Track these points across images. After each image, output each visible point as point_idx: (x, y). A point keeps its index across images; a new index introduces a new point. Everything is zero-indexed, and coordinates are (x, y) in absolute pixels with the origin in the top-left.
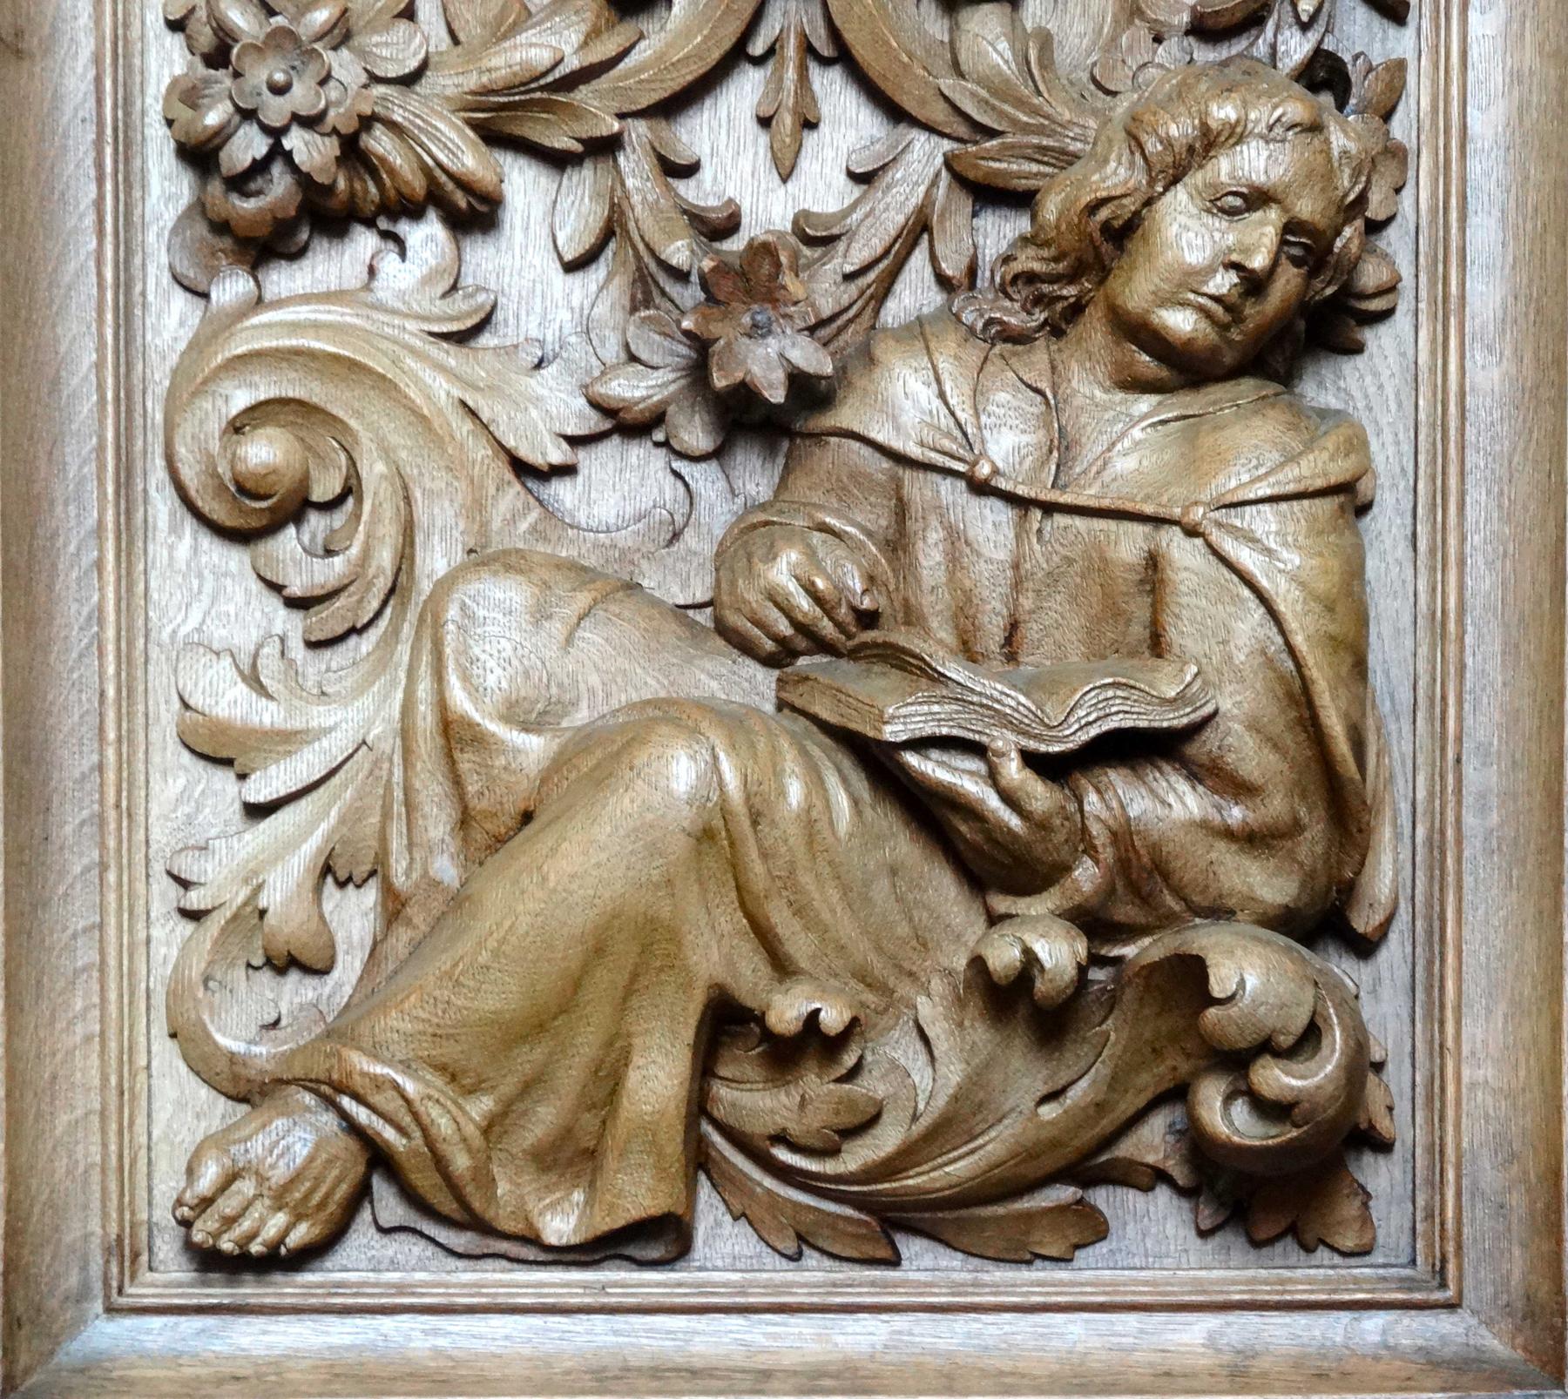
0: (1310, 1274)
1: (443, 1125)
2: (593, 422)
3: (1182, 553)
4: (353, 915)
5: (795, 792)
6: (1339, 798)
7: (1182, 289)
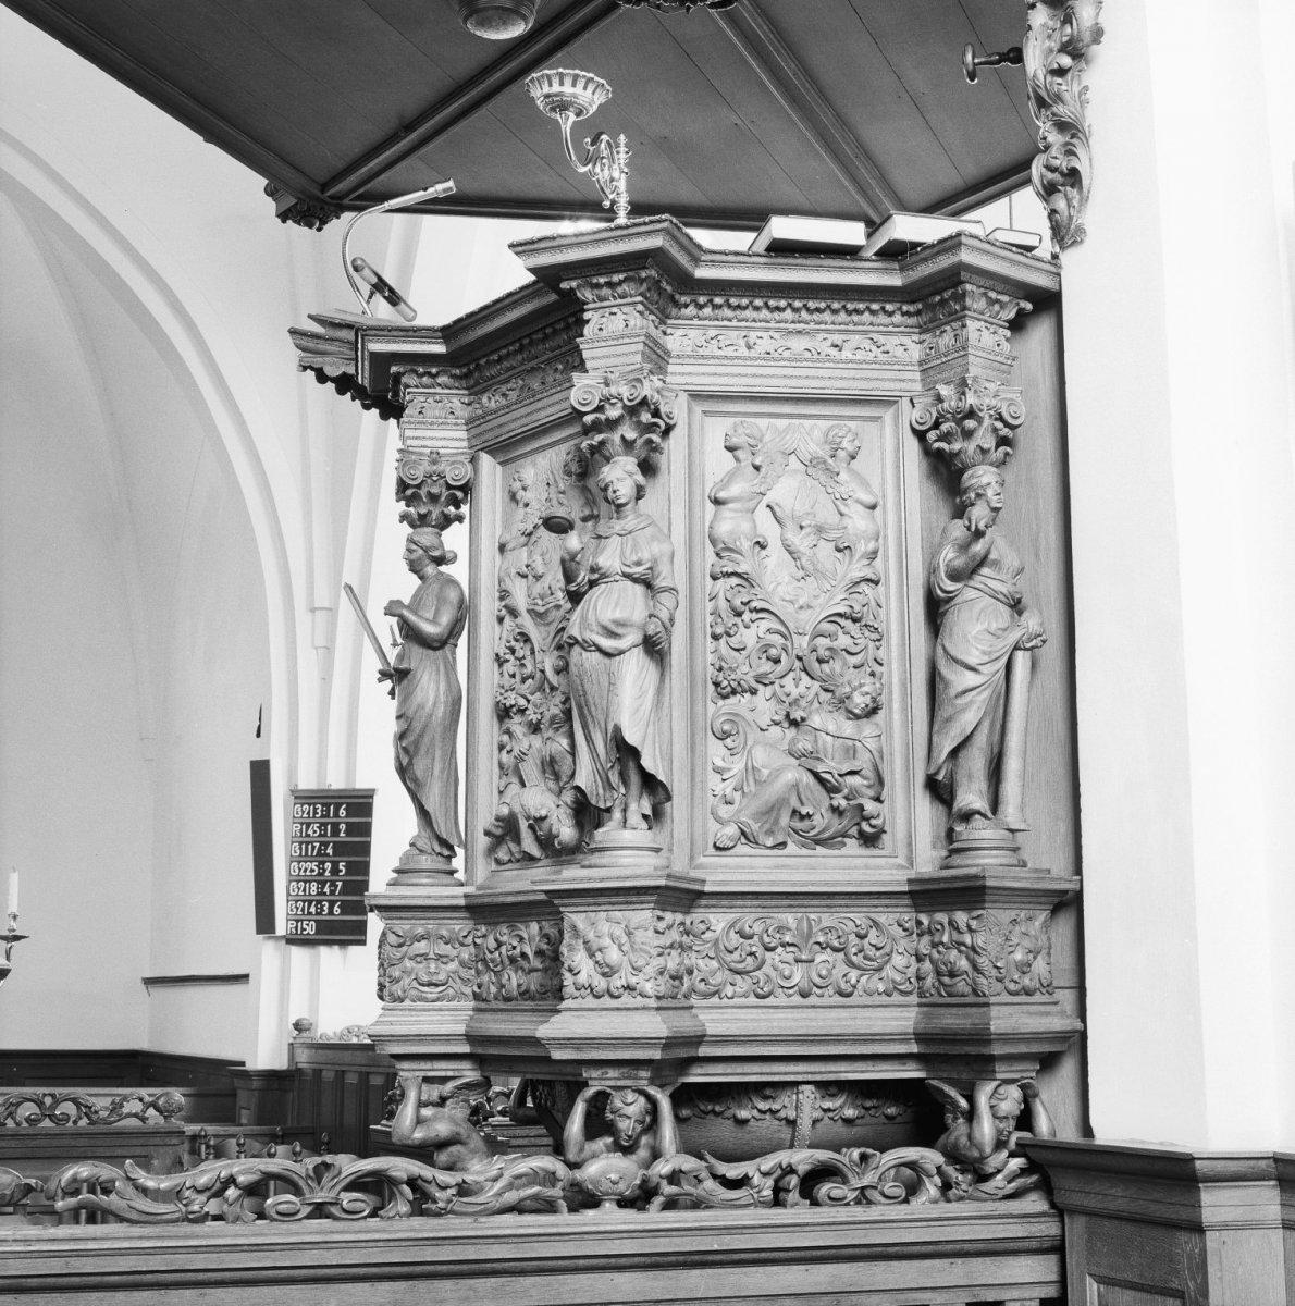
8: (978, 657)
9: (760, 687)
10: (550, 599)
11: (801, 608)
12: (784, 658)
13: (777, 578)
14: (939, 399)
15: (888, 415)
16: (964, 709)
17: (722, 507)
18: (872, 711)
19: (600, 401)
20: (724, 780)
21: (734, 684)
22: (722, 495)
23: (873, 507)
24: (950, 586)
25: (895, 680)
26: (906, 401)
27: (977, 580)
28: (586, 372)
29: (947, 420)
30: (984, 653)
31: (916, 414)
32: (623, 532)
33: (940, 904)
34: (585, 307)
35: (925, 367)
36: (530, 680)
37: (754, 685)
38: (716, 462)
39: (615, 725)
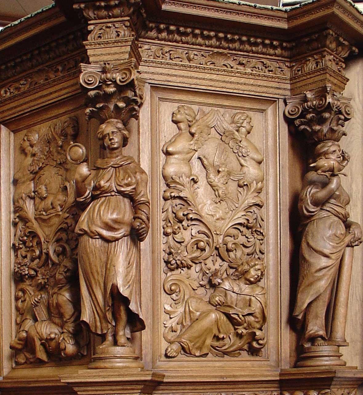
0: (258, 358)
1: (190, 345)
2: (199, 286)
3: (253, 298)
4: (179, 327)
5: (222, 318)
6: (264, 318)
7: (252, 277)
8: (329, 249)
9: (194, 265)
10: (52, 211)
11: (218, 219)
12: (207, 249)
13: (204, 202)
14: (305, 100)
15: (270, 110)
16: (319, 279)
17: (171, 156)
18: (258, 280)
19: (100, 82)
20: (171, 318)
21: (179, 262)
22: (170, 149)
23: (260, 163)
24: (312, 208)
25: (271, 263)
26: (281, 101)
27: (327, 207)
28: (90, 63)
29: (310, 113)
30: (334, 247)
31: (289, 108)
32: (116, 166)
33: (35, 344)
34: (89, 22)
35: (294, 81)
36: (38, 260)
37: (191, 263)
38: (168, 129)
39: (112, 285)
